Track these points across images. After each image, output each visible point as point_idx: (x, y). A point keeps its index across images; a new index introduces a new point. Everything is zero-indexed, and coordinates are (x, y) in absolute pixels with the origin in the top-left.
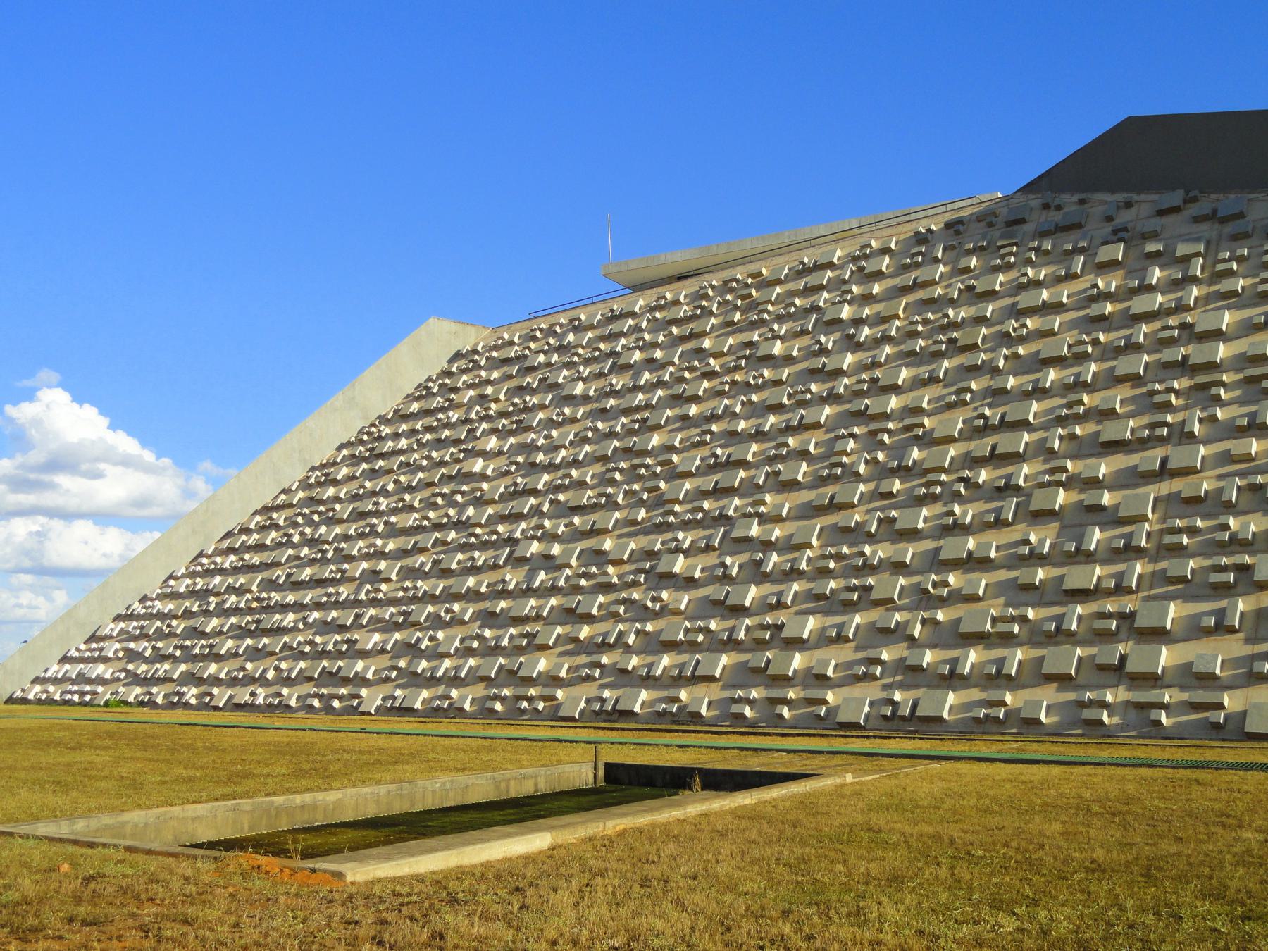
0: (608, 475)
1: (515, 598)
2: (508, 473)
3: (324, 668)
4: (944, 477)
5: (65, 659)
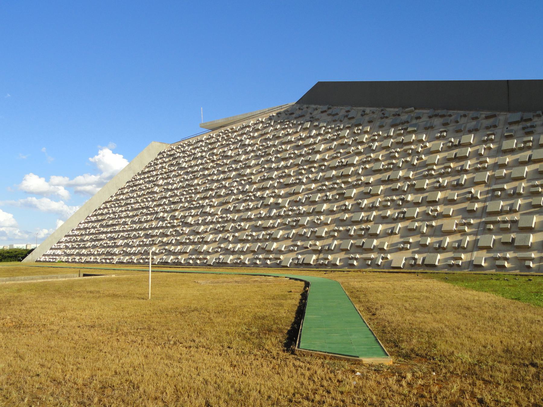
0: (300, 171)
1: (264, 220)
2: (261, 172)
3: (259, 246)
4: (435, 167)
5: (51, 249)
